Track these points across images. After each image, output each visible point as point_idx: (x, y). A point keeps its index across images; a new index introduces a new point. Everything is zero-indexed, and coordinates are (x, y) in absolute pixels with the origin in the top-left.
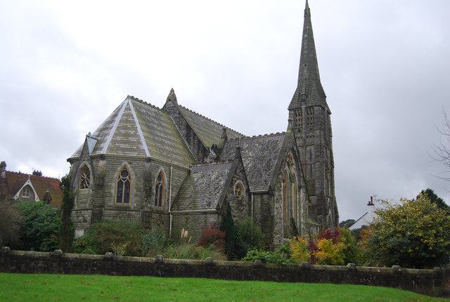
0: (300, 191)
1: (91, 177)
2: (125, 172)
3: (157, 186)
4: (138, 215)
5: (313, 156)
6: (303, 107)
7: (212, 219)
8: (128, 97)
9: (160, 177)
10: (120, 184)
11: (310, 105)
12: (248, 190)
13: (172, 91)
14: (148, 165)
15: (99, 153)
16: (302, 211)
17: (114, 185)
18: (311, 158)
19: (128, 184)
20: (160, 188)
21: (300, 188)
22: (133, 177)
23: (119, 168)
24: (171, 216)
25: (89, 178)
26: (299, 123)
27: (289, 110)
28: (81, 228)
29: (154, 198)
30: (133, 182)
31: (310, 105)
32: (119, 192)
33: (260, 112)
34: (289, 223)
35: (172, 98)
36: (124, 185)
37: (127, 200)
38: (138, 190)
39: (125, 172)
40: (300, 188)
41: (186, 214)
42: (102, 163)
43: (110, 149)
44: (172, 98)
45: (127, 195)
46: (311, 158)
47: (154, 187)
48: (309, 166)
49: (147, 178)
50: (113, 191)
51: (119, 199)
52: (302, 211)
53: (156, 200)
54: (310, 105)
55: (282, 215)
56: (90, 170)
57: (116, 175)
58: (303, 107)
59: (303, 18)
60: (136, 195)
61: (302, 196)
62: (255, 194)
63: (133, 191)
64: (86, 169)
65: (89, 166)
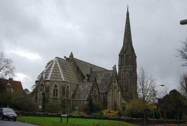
0: (118, 92)
1: (44, 88)
2: (56, 86)
3: (67, 91)
4: (60, 101)
5: (128, 76)
6: (125, 55)
7: (86, 103)
8: (56, 57)
9: (68, 88)
10: (54, 90)
11: (127, 55)
12: (99, 92)
13: (72, 53)
14: (63, 83)
15: (47, 79)
16: (119, 99)
17: (52, 91)
18: (127, 76)
19: (57, 90)
20: (68, 91)
21: (119, 91)
22: (59, 88)
23: (54, 85)
24: (71, 101)
25: (43, 88)
26: (123, 61)
27: (119, 56)
28: (40, 105)
29: (66, 95)
30: (59, 90)
31: (128, 55)
32: (54, 93)
33: (109, 61)
34: (114, 104)
35: (72, 55)
36: (55, 91)
37: (56, 96)
38: (60, 92)
39: (56, 86)
40: (119, 91)
41: (77, 100)
42: (48, 83)
43: (51, 78)
44: (72, 55)
45: (57, 94)
46: (127, 76)
47: (66, 91)
48: (126, 80)
49: (63, 88)
50: (52, 93)
51: (54, 95)
52: (119, 99)
53: (66, 95)
54: (128, 55)
55: (111, 101)
56: (44, 85)
57: (53, 87)
58: (125, 55)
59: (123, 45)
60: (60, 94)
61: (119, 93)
62: (101, 93)
63: (59, 93)
64: (42, 85)
65: (43, 84)
